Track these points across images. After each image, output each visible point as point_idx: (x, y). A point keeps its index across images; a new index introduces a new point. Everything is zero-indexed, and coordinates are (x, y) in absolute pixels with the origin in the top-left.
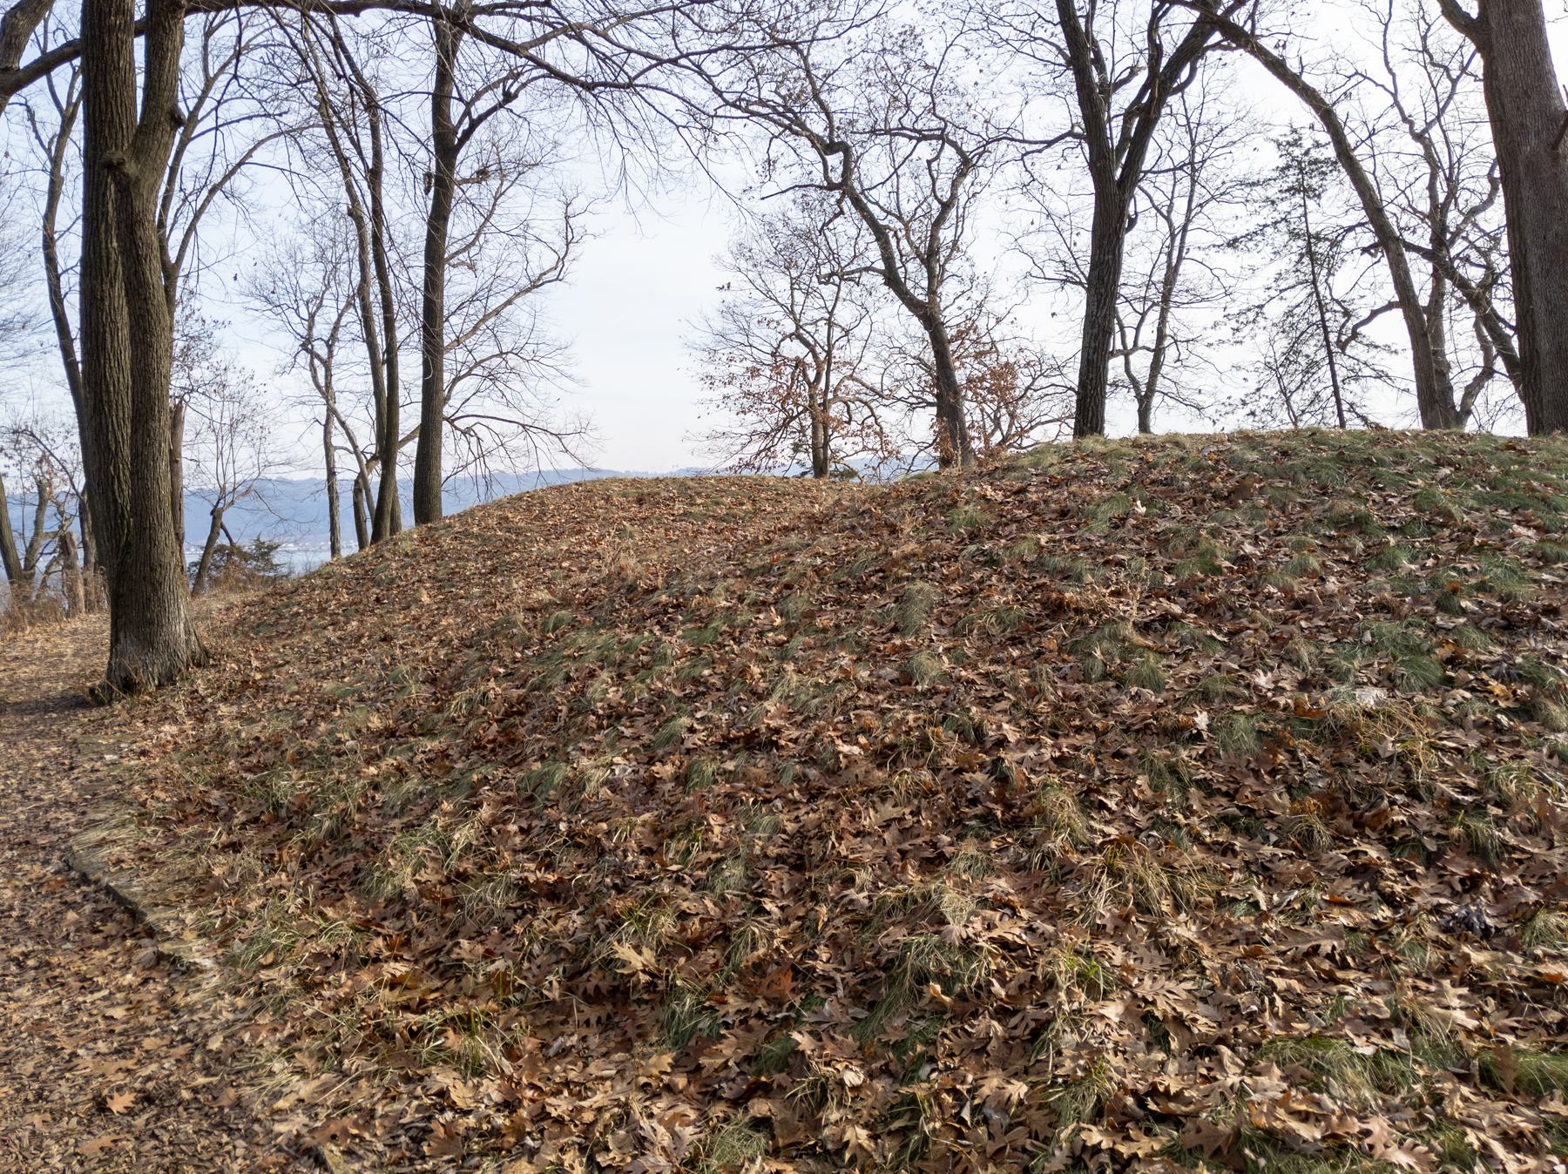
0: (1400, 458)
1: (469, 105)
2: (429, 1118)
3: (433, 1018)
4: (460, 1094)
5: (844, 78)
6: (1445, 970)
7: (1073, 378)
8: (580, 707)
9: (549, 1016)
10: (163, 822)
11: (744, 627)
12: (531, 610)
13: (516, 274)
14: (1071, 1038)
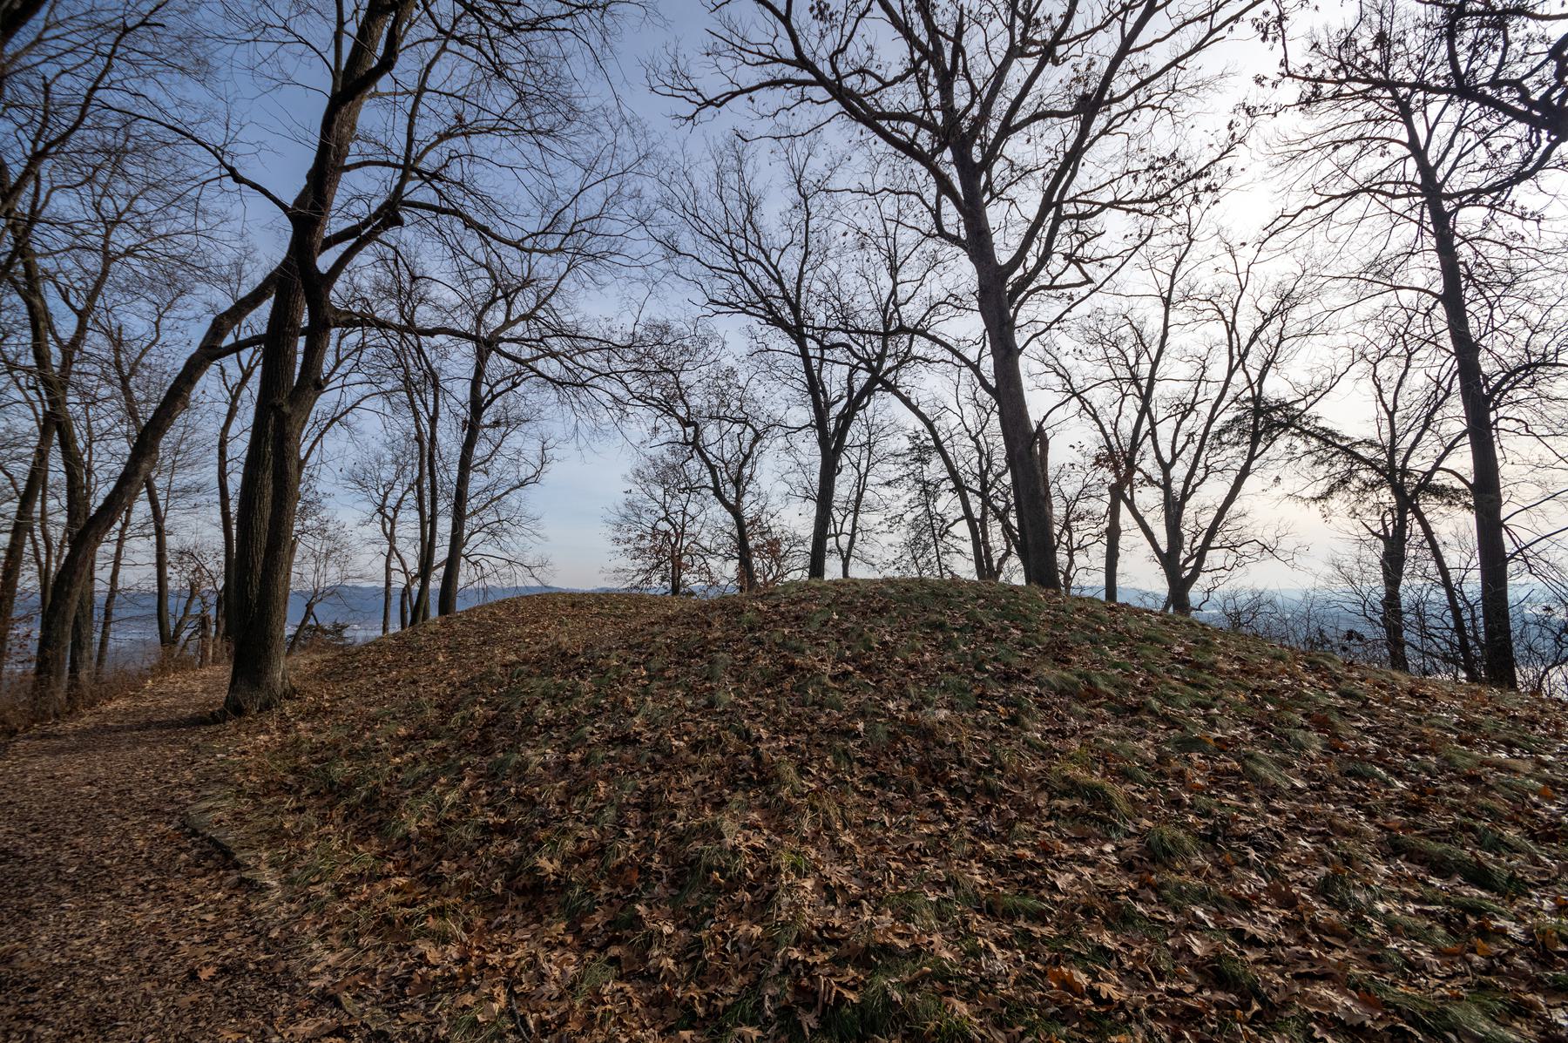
0: (961, 594)
1: (492, 387)
2: (411, 972)
3: (420, 910)
4: (433, 955)
5: (698, 390)
6: (972, 856)
7: (809, 548)
8: (529, 720)
9: (493, 904)
10: (253, 796)
11: (626, 676)
12: (505, 666)
13: (511, 477)
14: (787, 900)
